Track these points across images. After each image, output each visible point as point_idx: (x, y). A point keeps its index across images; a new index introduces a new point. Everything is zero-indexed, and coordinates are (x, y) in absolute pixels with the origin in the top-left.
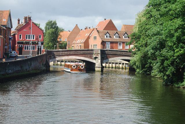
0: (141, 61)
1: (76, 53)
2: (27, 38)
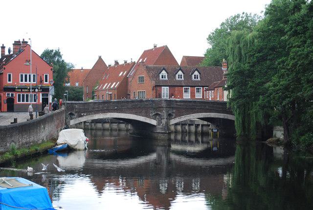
0: (6, 161)
1: (106, 106)
2: (22, 81)
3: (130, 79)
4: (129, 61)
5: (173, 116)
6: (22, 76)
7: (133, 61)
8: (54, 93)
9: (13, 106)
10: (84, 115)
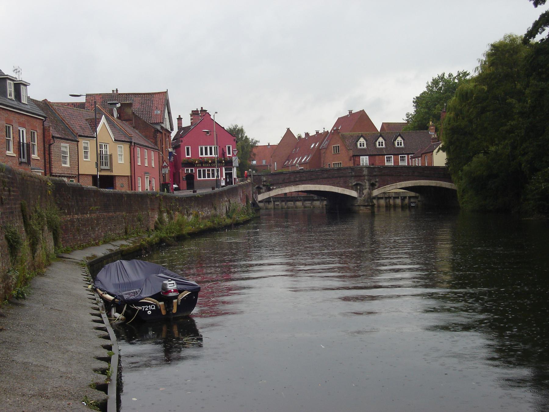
2: (202, 154)
3: (322, 152)
4: (321, 131)
5: (376, 185)
6: (202, 149)
7: (326, 130)
8: (238, 164)
9: (193, 184)
10: (273, 189)
